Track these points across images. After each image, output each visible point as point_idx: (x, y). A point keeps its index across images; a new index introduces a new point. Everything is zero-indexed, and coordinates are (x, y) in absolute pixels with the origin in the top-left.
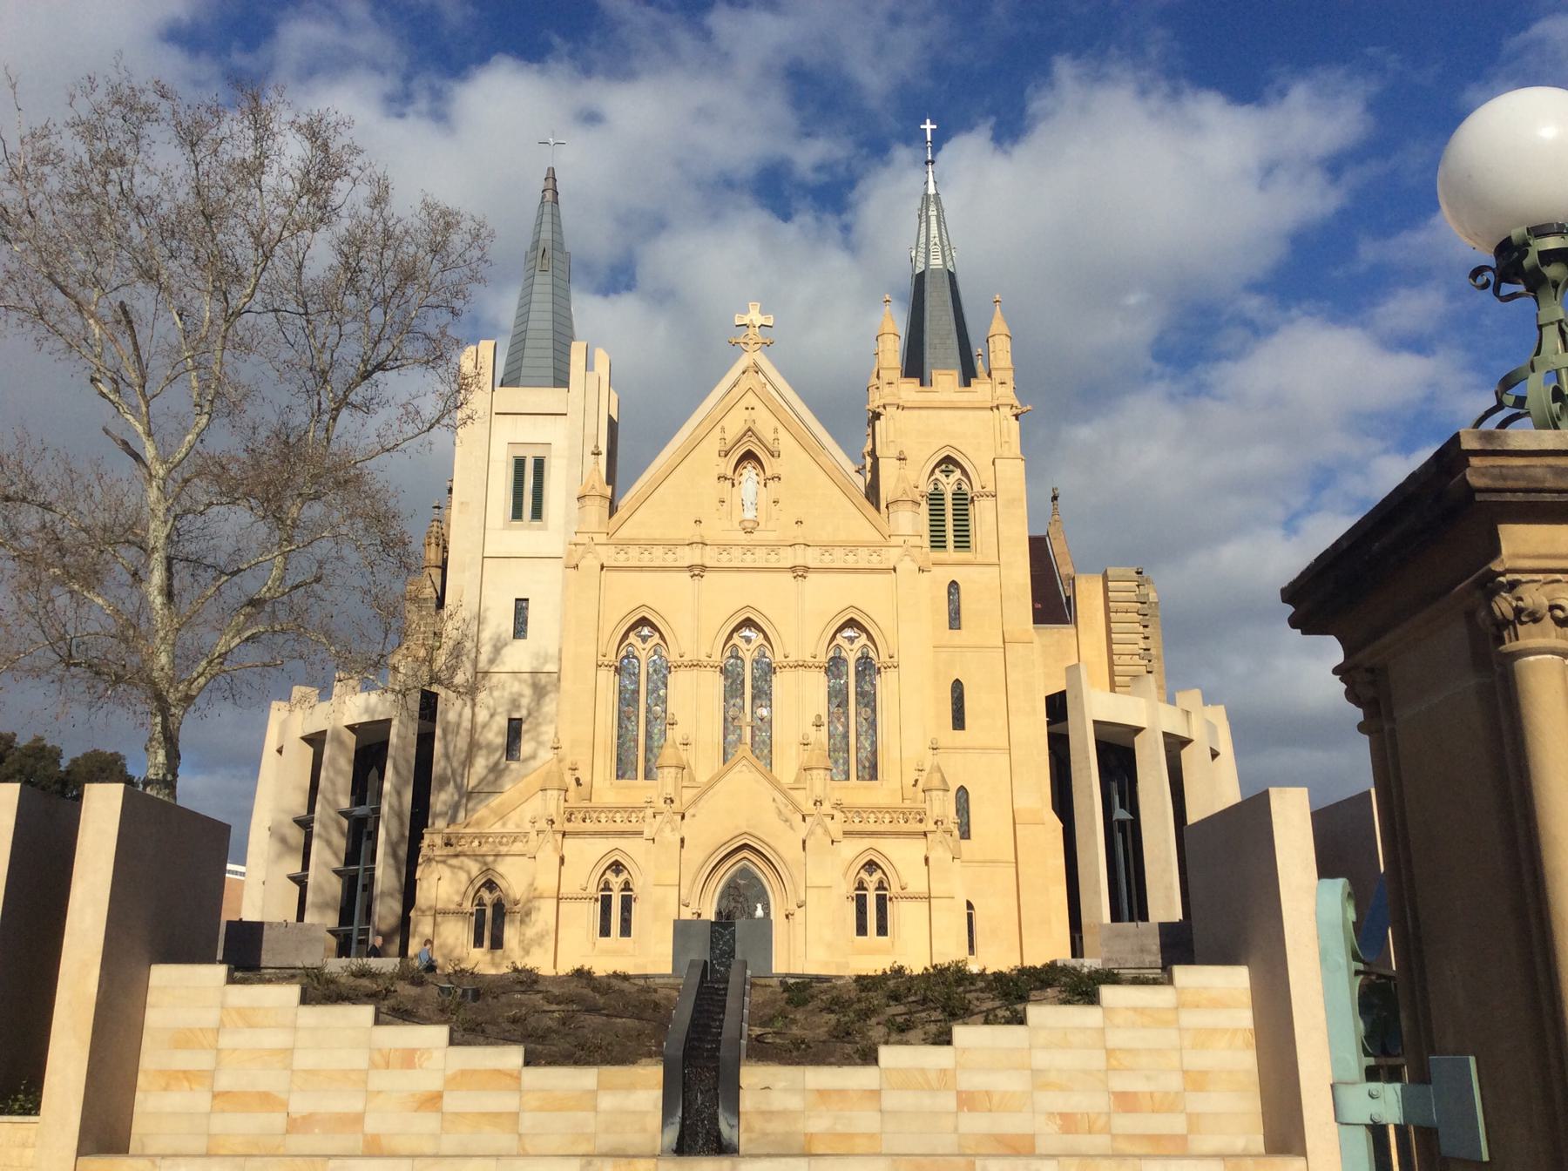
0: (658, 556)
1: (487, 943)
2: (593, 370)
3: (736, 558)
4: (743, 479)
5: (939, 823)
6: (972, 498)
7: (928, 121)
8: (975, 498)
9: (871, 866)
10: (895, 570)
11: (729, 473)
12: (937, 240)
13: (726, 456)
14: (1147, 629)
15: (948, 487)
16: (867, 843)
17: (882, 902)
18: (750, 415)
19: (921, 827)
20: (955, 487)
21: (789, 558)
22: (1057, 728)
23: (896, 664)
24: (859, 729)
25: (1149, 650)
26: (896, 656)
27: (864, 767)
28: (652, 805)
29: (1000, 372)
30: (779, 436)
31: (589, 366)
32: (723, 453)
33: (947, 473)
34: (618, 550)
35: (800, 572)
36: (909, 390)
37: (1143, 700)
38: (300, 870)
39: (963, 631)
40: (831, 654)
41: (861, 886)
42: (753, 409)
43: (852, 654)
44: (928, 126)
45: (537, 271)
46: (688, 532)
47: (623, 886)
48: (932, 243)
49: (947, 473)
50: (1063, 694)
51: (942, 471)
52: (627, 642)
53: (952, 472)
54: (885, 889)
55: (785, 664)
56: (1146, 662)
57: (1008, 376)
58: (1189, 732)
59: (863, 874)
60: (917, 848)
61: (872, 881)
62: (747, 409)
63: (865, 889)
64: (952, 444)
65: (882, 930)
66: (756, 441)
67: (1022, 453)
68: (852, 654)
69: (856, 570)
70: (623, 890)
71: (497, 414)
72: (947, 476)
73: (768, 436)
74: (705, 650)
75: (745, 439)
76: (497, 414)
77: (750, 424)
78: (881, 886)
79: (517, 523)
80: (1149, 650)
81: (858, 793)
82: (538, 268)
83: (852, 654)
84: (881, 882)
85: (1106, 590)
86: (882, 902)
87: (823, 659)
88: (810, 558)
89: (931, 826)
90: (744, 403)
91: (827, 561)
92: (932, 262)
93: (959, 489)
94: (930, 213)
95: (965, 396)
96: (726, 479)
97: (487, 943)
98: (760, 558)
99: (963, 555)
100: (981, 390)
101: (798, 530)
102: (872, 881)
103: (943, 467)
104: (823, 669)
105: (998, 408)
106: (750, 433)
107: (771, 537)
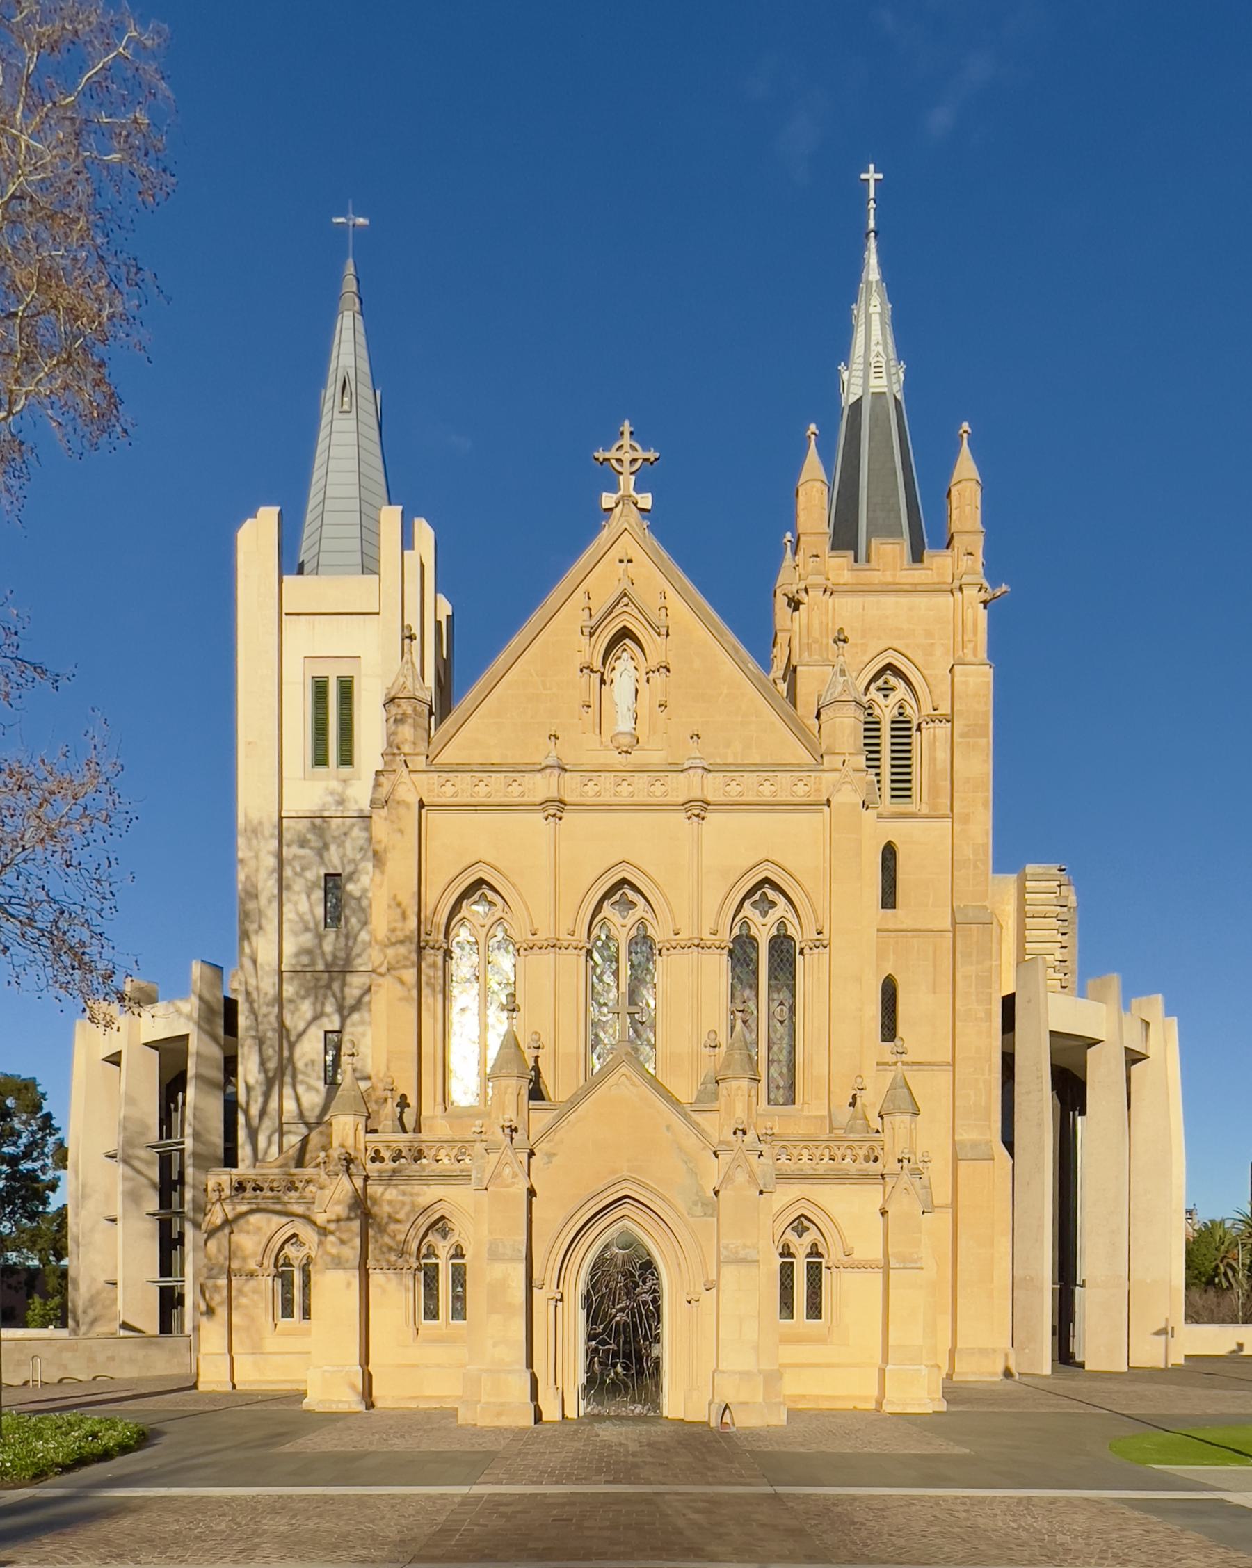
0: (494, 787)
1: (297, 1311)
2: (411, 547)
3: (604, 789)
4: (615, 675)
5: (905, 1162)
6: (919, 725)
7: (863, 176)
8: (923, 725)
9: (800, 1225)
10: (828, 803)
11: (597, 665)
12: (880, 348)
13: (591, 635)
14: (1065, 937)
15: (887, 711)
16: (795, 1191)
17: (814, 1273)
18: (626, 570)
19: (877, 1168)
20: (895, 711)
21: (683, 787)
22: (1008, 1036)
23: (825, 943)
24: (772, 1035)
25: (1065, 961)
26: (826, 931)
27: (778, 1087)
28: (483, 1137)
29: (966, 538)
30: (668, 603)
31: (407, 542)
32: (587, 631)
33: (886, 690)
34: (443, 781)
35: (699, 808)
36: (839, 567)
37: (1104, 1006)
38: (158, 1208)
39: (899, 911)
40: (736, 931)
41: (786, 1252)
42: (630, 561)
43: (763, 932)
44: (872, 175)
45: (337, 415)
46: (545, 752)
47: (452, 1252)
48: (873, 354)
49: (886, 690)
50: (1014, 994)
51: (879, 689)
52: (459, 916)
53: (892, 689)
54: (820, 1255)
55: (674, 944)
56: (1061, 976)
57: (978, 544)
58: (1146, 1050)
59: (791, 1237)
60: (873, 1196)
61: (801, 1247)
62: (621, 561)
63: (792, 1256)
64: (895, 646)
65: (815, 1310)
66: (635, 612)
67: (989, 657)
68: (763, 932)
69: (474, 807)
70: (453, 1257)
71: (287, 614)
72: (886, 696)
73: (651, 603)
74: (566, 924)
75: (618, 610)
76: (287, 614)
77: (625, 584)
78: (815, 1252)
79: (321, 770)
80: (1065, 961)
81: (777, 1120)
82: (336, 410)
83: (764, 930)
84: (815, 1245)
85: (1022, 891)
86: (814, 1273)
87: (725, 937)
88: (713, 787)
89: (894, 1167)
90: (615, 553)
91: (734, 793)
92: (873, 382)
93: (901, 714)
94: (872, 309)
95: (918, 575)
96: (592, 671)
97: (297, 1311)
98: (639, 788)
99: (902, 806)
100: (939, 564)
101: (693, 748)
102: (801, 1247)
103: (880, 682)
104: (726, 951)
105: (961, 589)
106: (625, 600)
107: (656, 758)
